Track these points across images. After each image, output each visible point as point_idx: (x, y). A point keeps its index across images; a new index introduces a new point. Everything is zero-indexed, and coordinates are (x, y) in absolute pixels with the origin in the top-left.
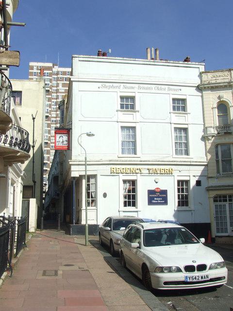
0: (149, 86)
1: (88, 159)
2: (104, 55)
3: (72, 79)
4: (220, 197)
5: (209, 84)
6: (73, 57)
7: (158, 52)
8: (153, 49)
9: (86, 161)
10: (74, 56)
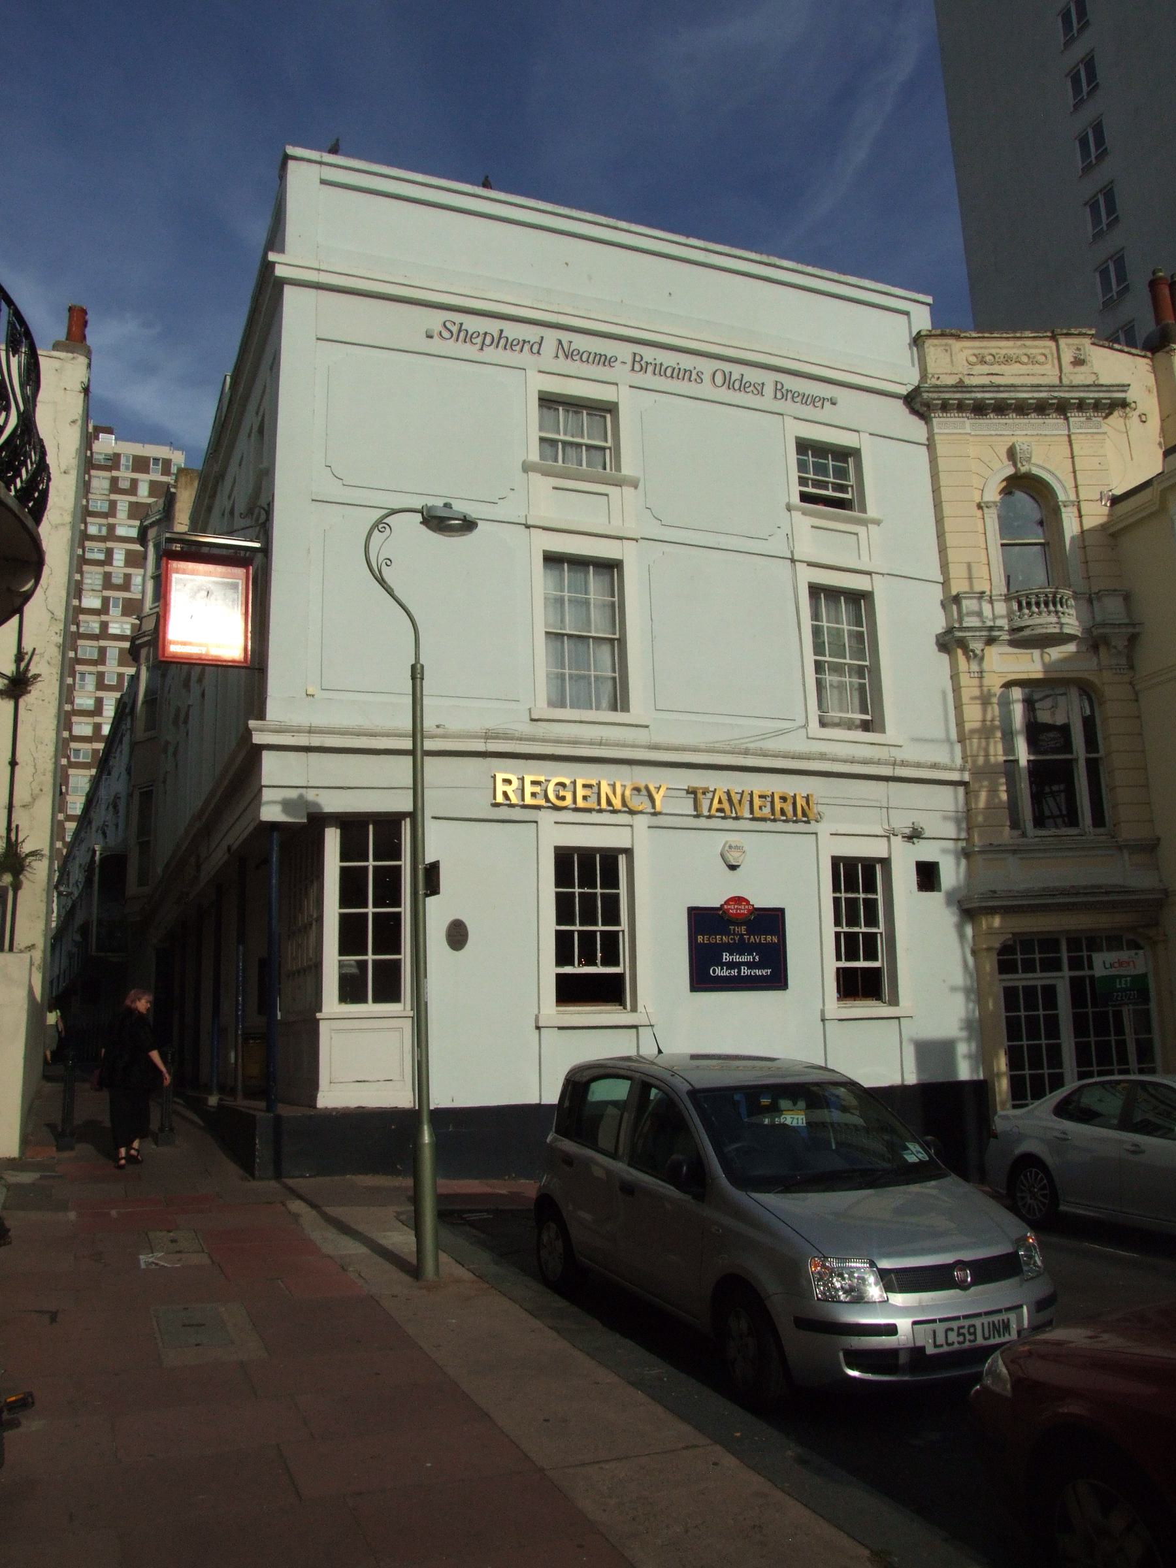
0: (687, 362)
1: (429, 724)
3: (280, 271)
5: (960, 386)
6: (287, 158)
9: (417, 732)
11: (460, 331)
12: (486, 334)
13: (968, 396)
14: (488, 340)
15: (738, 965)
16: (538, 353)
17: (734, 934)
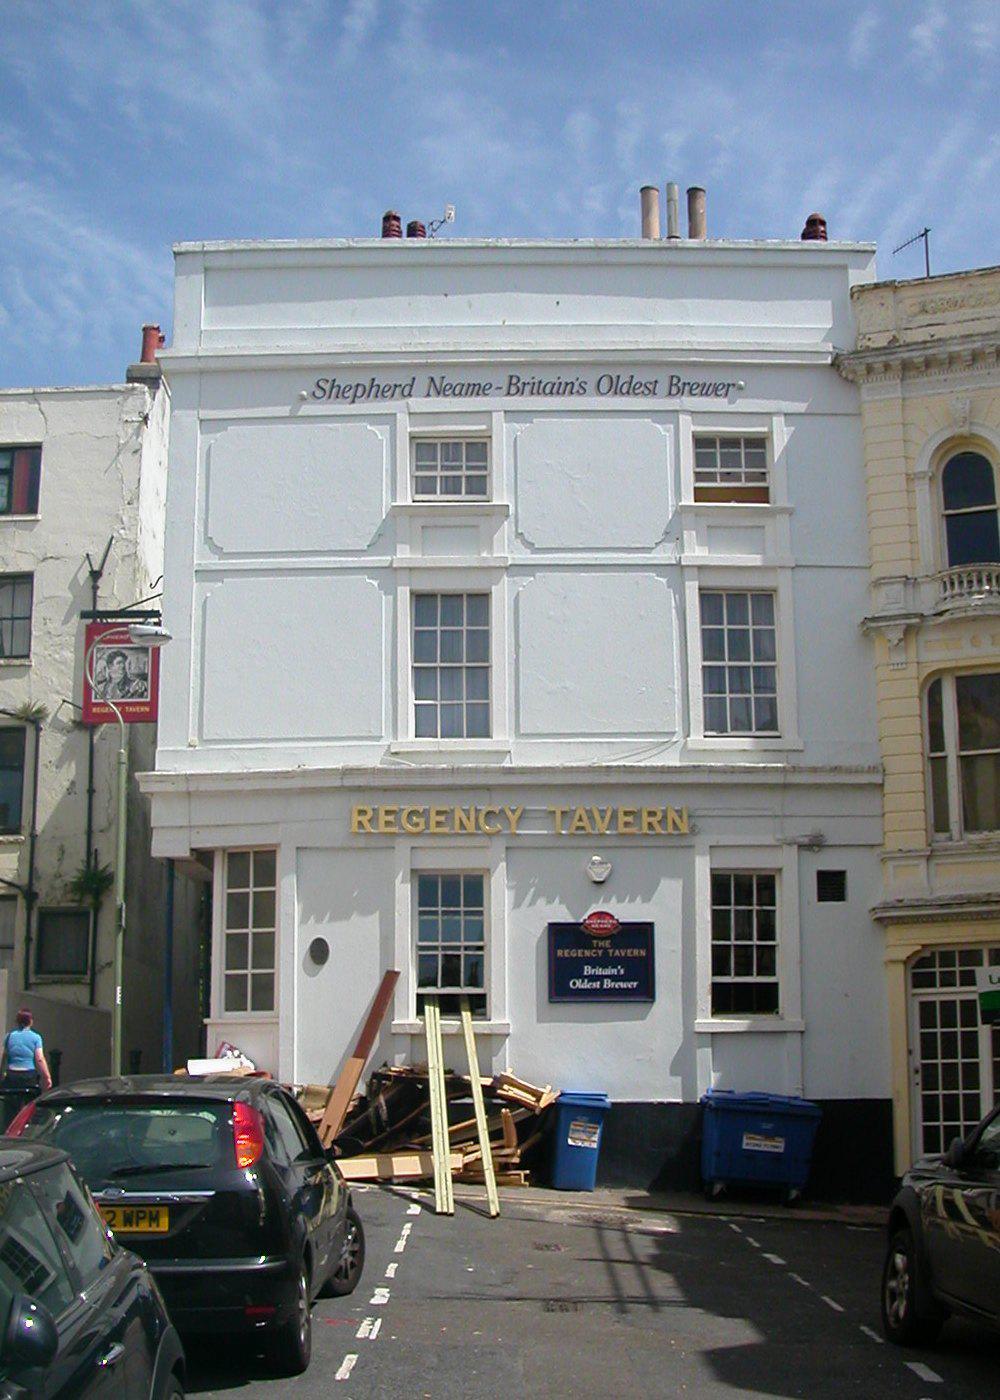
4: (947, 958)
11: (333, 387)
12: (358, 385)
13: (893, 357)
15: (601, 978)
17: (598, 948)
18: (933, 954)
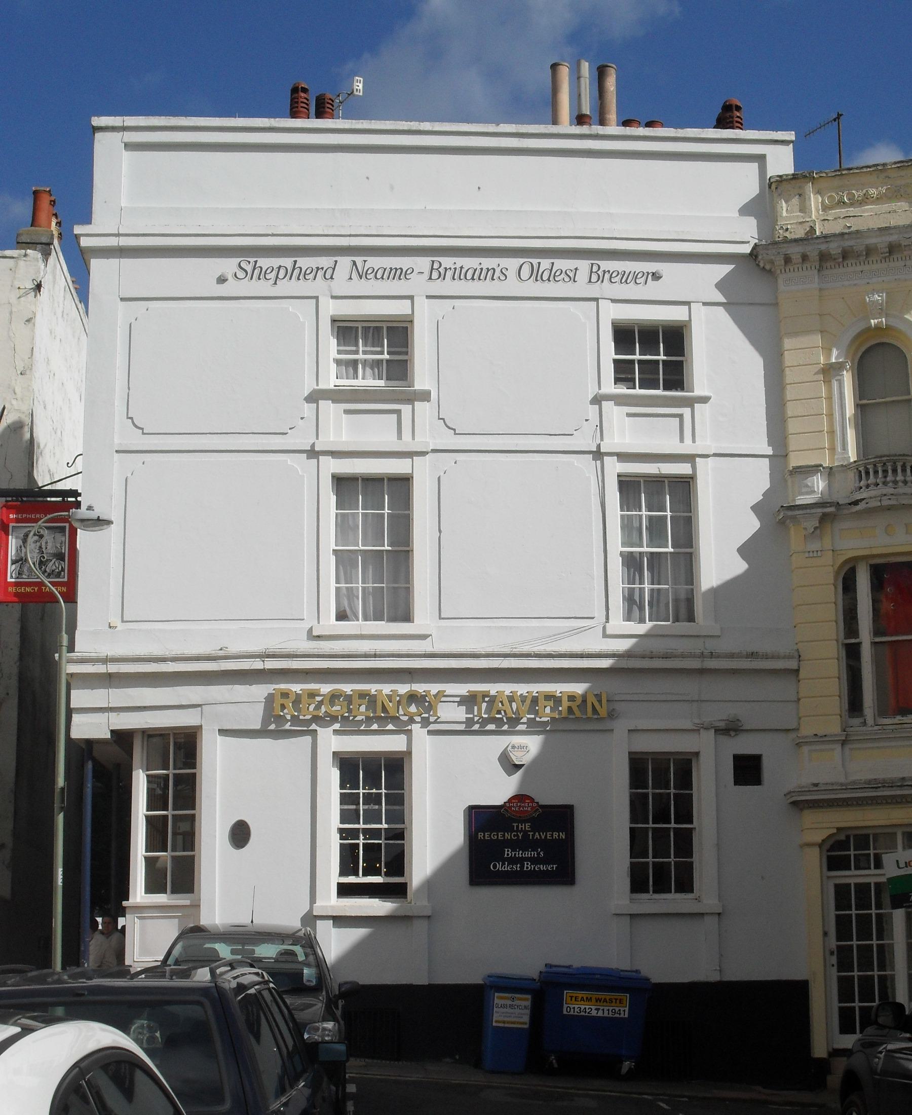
2: (323, 109)
7: (611, 83)
8: (585, 67)
10: (97, 121)
14: (282, 273)
15: (521, 861)
16: (332, 278)
17: (517, 831)
18: (848, 837)
